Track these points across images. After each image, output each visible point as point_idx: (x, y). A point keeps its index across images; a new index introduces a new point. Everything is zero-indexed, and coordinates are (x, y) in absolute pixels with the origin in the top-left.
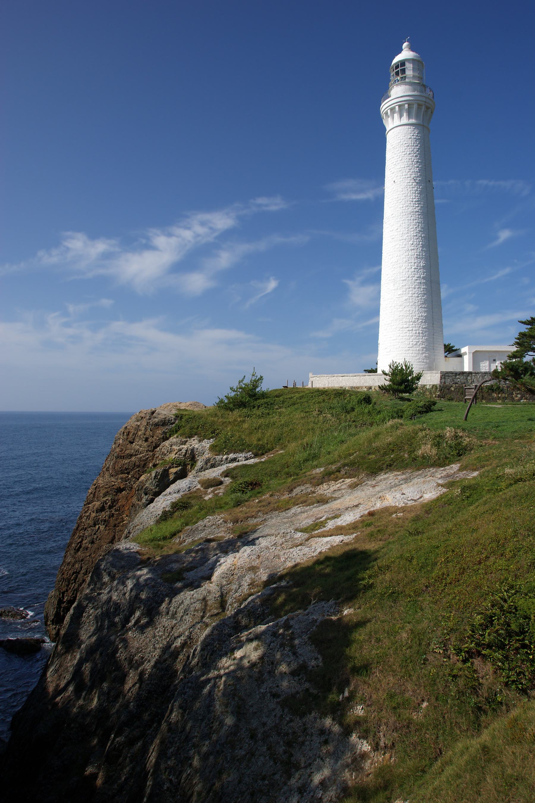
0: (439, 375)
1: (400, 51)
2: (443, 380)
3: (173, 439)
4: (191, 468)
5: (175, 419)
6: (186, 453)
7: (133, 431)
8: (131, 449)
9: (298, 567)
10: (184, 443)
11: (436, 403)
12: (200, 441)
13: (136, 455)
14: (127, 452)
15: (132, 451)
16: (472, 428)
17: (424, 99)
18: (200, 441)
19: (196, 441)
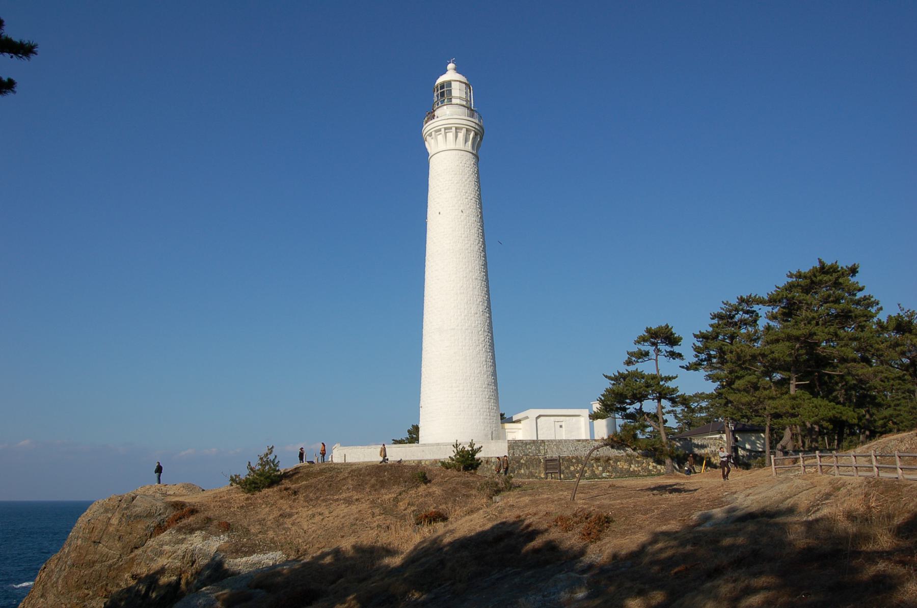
0: (506, 445)
1: (445, 71)
2: (512, 451)
3: (165, 537)
4: (838, 445)
5: (166, 508)
6: (184, 557)
7: (100, 526)
8: (95, 553)
9: (531, 529)
10: (182, 541)
11: (613, 521)
12: (205, 538)
13: (102, 562)
14: (89, 557)
15: (97, 556)
16: (844, 404)
17: (473, 125)
18: (205, 538)
19: (199, 539)
